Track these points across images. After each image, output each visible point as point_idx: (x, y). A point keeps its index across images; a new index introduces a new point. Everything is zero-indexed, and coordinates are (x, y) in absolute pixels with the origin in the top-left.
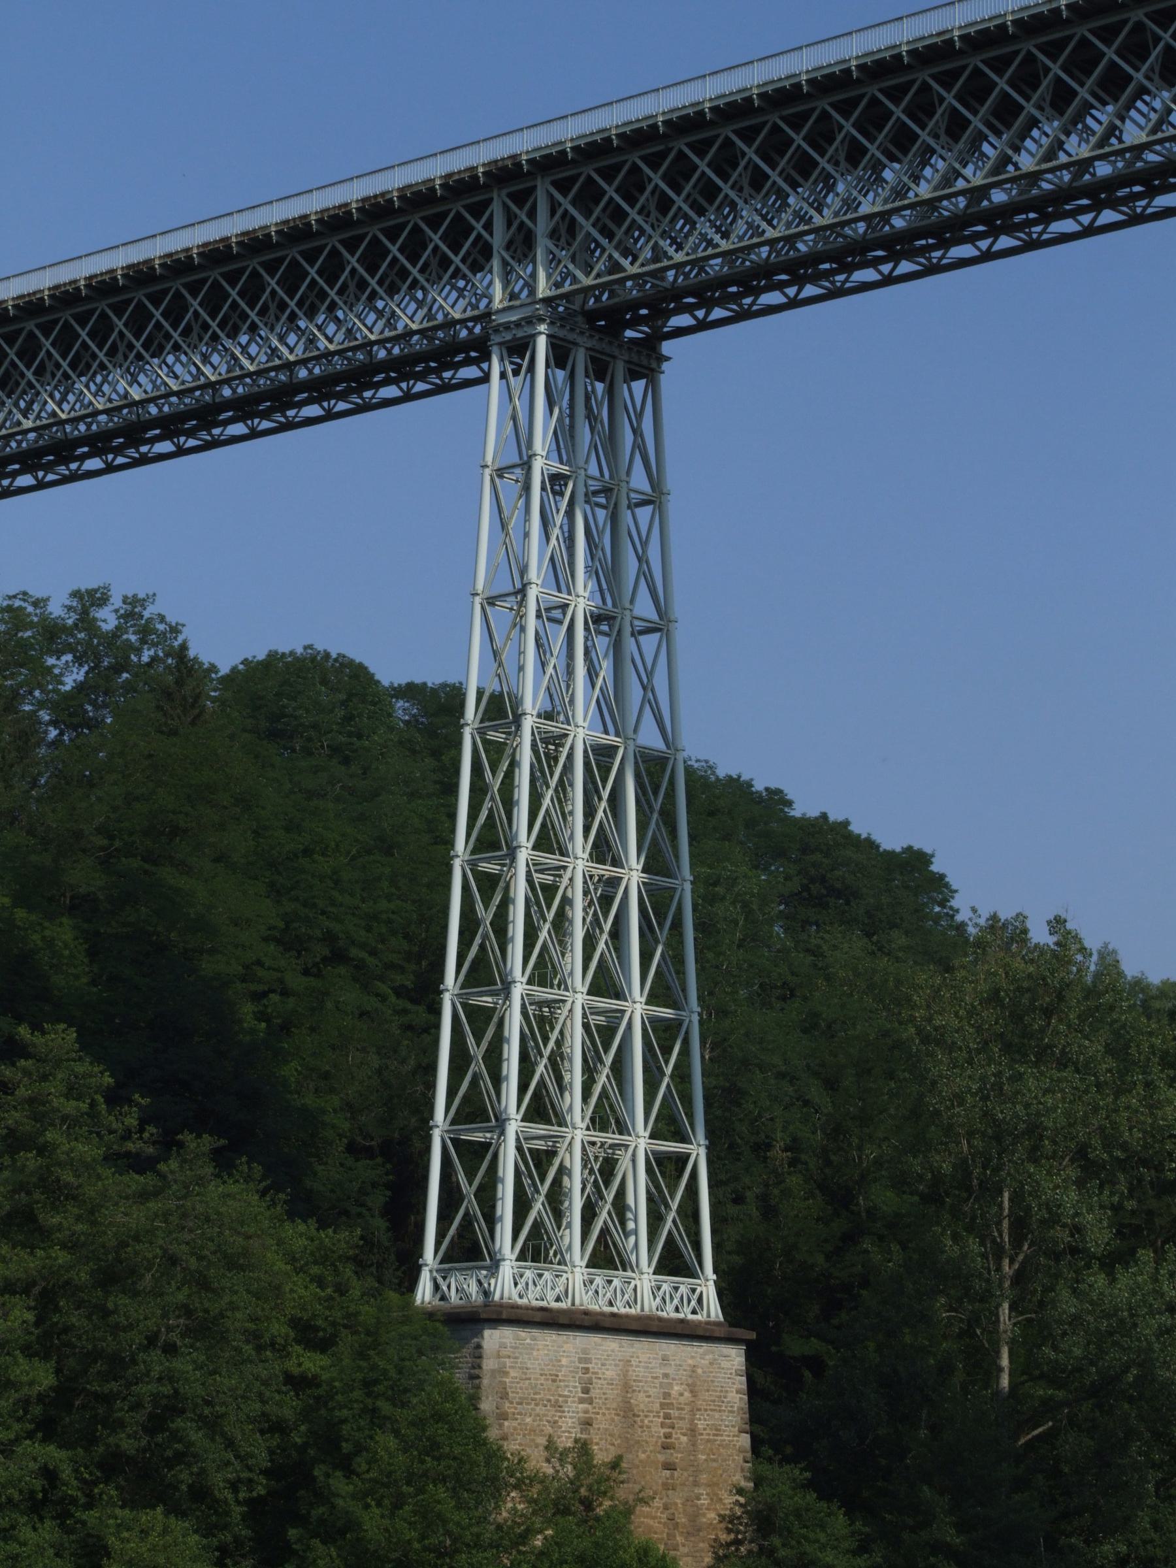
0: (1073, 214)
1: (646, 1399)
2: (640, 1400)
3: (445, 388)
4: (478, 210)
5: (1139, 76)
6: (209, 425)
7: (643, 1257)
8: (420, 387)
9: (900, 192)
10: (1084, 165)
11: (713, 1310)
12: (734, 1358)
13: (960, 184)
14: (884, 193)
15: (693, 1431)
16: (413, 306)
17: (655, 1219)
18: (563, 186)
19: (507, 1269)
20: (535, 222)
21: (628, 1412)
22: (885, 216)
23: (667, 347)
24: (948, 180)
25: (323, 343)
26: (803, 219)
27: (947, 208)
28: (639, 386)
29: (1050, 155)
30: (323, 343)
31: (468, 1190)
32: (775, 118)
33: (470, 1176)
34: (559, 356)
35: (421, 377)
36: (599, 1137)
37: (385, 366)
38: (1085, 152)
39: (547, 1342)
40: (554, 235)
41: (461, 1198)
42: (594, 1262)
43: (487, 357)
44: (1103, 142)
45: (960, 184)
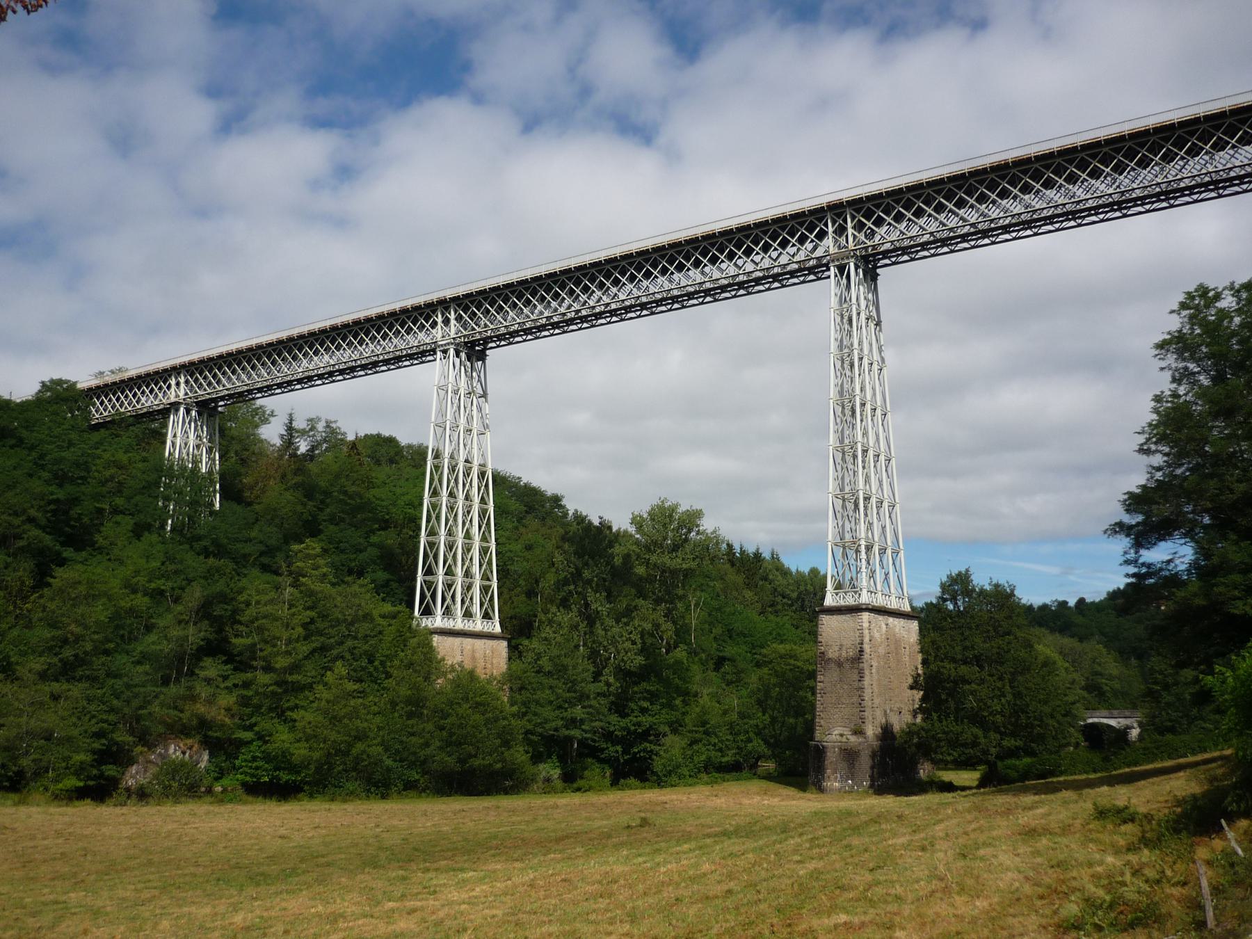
0: (665, 305)
1: (479, 655)
2: (477, 655)
3: (423, 362)
4: (434, 312)
5: (740, 253)
6: (353, 372)
7: (439, 610)
8: (416, 362)
9: (556, 310)
10: (608, 305)
11: (498, 629)
12: (505, 643)
13: (573, 309)
14: (551, 310)
15: (492, 664)
16: (1224, 162)
17: (482, 605)
18: (459, 306)
19: (439, 619)
20: (827, 227)
21: (474, 658)
22: (551, 317)
23: (488, 352)
24: (569, 307)
25: (387, 349)
26: (529, 317)
27: (569, 316)
28: (480, 363)
29: (598, 301)
30: (387, 349)
31: (428, 595)
32: (520, 288)
33: (429, 590)
34: (458, 354)
35: (416, 359)
36: (466, 580)
37: (405, 356)
38: (608, 301)
39: (450, 641)
40: (456, 319)
41: (426, 597)
42: (484, 617)
43: (435, 353)
44: (613, 298)
45: (573, 309)
